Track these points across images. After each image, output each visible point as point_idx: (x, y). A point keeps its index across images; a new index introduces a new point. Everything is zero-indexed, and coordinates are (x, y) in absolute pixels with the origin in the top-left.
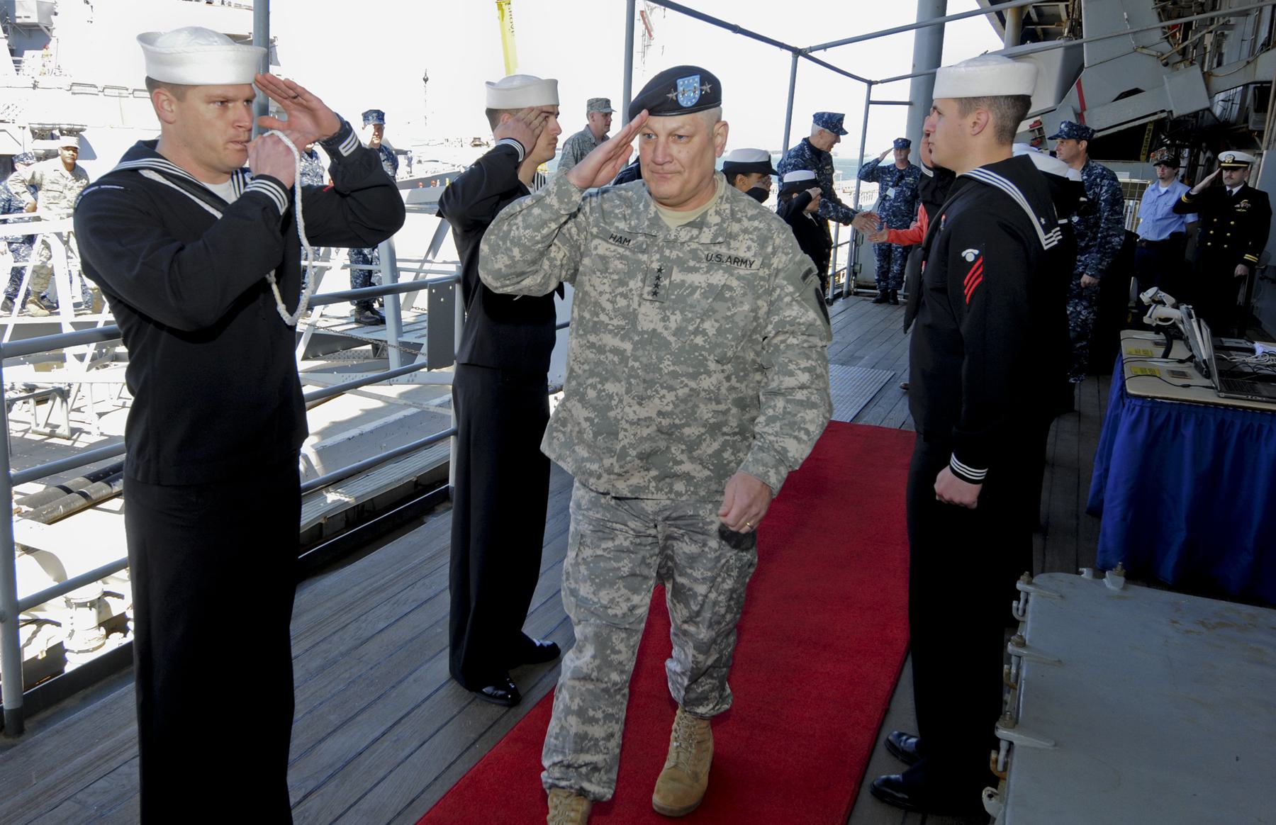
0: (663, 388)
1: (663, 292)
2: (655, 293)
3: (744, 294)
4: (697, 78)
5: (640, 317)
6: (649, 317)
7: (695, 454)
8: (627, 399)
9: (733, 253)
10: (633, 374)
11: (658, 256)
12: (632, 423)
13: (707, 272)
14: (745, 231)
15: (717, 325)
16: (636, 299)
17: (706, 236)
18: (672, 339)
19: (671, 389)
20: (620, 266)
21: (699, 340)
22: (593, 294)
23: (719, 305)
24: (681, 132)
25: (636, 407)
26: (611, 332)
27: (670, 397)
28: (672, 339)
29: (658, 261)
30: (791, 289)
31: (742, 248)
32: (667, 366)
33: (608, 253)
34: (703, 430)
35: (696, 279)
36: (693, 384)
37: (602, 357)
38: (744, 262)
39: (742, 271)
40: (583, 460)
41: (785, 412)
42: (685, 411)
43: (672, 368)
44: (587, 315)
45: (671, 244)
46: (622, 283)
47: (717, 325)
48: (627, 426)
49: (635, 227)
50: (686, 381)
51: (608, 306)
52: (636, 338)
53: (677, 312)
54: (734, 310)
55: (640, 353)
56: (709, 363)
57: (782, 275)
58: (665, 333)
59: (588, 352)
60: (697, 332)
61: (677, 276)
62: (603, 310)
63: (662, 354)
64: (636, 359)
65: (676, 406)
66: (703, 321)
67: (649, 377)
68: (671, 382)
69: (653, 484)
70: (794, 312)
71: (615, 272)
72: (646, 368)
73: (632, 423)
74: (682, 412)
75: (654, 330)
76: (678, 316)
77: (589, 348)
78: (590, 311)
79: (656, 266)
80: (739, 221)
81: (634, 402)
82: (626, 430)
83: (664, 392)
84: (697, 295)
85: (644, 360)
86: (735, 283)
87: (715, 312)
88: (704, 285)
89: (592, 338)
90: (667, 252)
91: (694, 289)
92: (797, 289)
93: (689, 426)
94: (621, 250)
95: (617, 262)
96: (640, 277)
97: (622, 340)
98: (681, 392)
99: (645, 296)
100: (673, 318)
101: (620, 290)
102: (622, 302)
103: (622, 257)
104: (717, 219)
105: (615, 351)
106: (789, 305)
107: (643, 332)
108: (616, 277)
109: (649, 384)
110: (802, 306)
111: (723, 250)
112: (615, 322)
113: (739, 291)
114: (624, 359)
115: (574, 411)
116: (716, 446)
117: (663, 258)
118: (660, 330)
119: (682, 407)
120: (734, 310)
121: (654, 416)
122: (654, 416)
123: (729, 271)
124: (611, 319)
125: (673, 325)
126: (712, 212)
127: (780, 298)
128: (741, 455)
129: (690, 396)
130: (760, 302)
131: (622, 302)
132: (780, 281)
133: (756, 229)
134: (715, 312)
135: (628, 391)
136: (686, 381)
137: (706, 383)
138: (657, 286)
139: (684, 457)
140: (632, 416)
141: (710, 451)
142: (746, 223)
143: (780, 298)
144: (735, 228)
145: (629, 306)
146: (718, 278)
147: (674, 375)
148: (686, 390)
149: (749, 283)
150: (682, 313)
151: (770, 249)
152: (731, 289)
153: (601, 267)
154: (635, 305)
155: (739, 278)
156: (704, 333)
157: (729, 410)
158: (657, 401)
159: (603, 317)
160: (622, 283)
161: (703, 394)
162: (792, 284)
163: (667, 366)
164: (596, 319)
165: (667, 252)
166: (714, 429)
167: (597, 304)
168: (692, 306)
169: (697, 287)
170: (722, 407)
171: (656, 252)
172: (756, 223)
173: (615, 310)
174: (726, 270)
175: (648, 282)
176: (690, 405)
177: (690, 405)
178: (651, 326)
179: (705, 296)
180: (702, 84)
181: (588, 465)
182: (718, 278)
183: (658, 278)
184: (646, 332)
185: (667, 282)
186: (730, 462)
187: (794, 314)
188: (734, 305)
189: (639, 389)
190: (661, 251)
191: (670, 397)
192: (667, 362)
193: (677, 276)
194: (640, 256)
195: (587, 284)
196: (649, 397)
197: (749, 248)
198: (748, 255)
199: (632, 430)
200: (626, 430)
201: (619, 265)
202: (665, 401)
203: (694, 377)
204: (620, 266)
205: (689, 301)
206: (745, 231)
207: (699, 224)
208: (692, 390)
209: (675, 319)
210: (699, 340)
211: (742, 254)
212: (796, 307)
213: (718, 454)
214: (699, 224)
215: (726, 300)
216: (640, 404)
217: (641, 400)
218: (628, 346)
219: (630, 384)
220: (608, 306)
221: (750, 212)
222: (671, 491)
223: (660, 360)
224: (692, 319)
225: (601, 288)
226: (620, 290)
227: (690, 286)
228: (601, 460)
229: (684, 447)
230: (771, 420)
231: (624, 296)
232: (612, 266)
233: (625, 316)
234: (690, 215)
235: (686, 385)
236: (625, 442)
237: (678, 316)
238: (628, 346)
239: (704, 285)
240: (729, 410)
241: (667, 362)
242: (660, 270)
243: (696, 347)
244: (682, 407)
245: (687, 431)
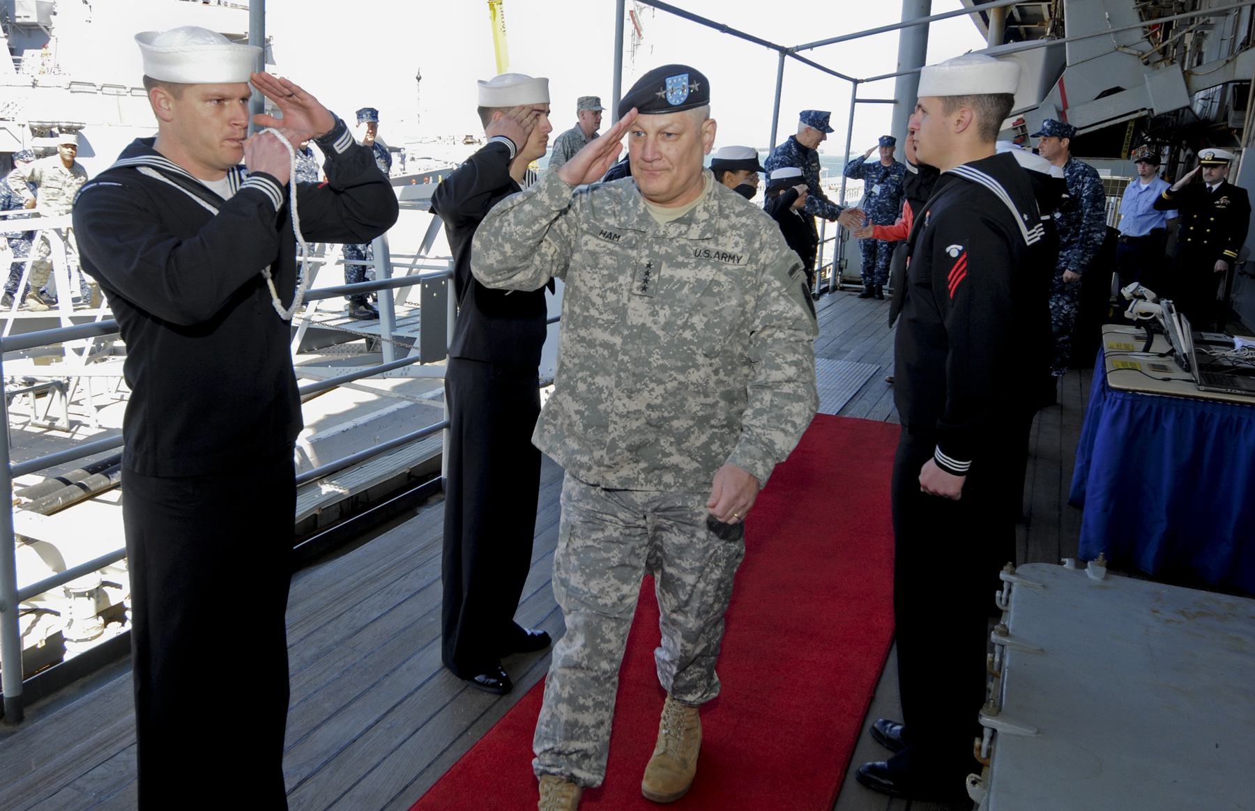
0: (652, 381)
1: (652, 287)
2: (644, 289)
3: (732, 289)
4: (686, 77)
5: (630, 311)
6: (638, 312)
7: (684, 446)
8: (616, 392)
9: (720, 248)
10: (622, 368)
11: (647, 252)
12: (621, 416)
13: (696, 267)
14: (733, 227)
15: (705, 319)
16: (626, 294)
17: (695, 232)
18: (661, 333)
19: (660, 382)
20: (610, 262)
21: (688, 335)
22: (584, 289)
23: (707, 300)
24: (670, 130)
25: (626, 401)
26: (600, 326)
27: (659, 390)
28: (661, 333)
29: (647, 256)
30: (778, 284)
31: (730, 243)
32: (656, 359)
33: (598, 249)
34: (691, 423)
35: (685, 274)
36: (681, 378)
38: (732, 257)
39: (730, 266)
40: (574, 452)
41: (772, 405)
42: (674, 404)
43: (660, 362)
44: (577, 310)
45: (660, 239)
46: (612, 278)
47: (705, 319)
48: (617, 419)
50: (675, 375)
51: (598, 301)
52: (626, 332)
53: (666, 307)
54: (722, 305)
55: (629, 347)
56: (698, 357)
57: (769, 270)
58: (654, 328)
59: (578, 346)
60: (685, 326)
61: (666, 271)
62: (593, 305)
63: (652, 348)
64: (625, 353)
65: (665, 399)
66: (691, 315)
67: (638, 371)
68: (660, 376)
69: (642, 476)
70: (780, 306)
71: (605, 267)
72: (636, 362)
73: (621, 416)
74: (670, 405)
75: (644, 325)
76: (667, 311)
77: (579, 342)
78: (580, 306)
79: (645, 261)
80: (727, 217)
81: (624, 396)
82: (615, 423)
83: (653, 385)
84: (686, 290)
85: (634, 354)
86: (723, 278)
87: (703, 306)
88: (692, 280)
89: (583, 333)
90: (656, 248)
91: (682, 284)
92: (784, 284)
93: (678, 418)
94: (611, 246)
95: (607, 258)
96: (629, 272)
97: (612, 334)
98: (670, 386)
99: (635, 291)
100: (662, 313)
101: (610, 285)
102: (611, 297)
103: (612, 253)
104: (705, 216)
105: (605, 345)
106: (776, 300)
107: (633, 326)
108: (605, 272)
109: (639, 377)
110: (788, 301)
111: (711, 246)
112: (605, 317)
113: (727, 286)
114: (614, 353)
116: (704, 438)
117: (652, 254)
118: (649, 324)
119: (671, 400)
120: (722, 305)
121: (643, 409)
122: (643, 409)
123: (717, 267)
124: (601, 313)
125: (662, 320)
126: (700, 208)
127: (767, 293)
128: (729, 447)
129: (679, 389)
130: (747, 297)
131: (611, 297)
132: (767, 276)
133: (744, 225)
134: (703, 306)
135: (618, 385)
136: (675, 375)
137: (695, 376)
138: (646, 281)
139: (672, 449)
140: (621, 409)
141: (698, 443)
142: (733, 219)
143: (767, 293)
144: (723, 224)
145: (618, 301)
146: (707, 273)
147: (663, 368)
148: (675, 384)
149: (737, 278)
150: (671, 308)
151: (757, 245)
152: (719, 284)
153: (591, 263)
154: (625, 300)
155: (727, 273)
156: (692, 327)
157: (717, 403)
158: (646, 394)
159: (593, 312)
160: (612, 278)
161: (691, 387)
162: (779, 279)
163: (656, 359)
164: (586, 314)
165: (656, 248)
166: (702, 422)
167: (587, 299)
168: (680, 301)
169: (686, 282)
170: (710, 400)
171: (646, 248)
172: (744, 220)
173: (605, 305)
174: (714, 266)
175: (637, 277)
176: (679, 398)
177: (679, 398)
178: (641, 321)
179: (693, 291)
180: (690, 82)
182: (707, 273)
183: (647, 273)
184: (635, 326)
185: (656, 277)
186: (718, 454)
187: (781, 308)
188: (722, 300)
189: (628, 383)
190: (650, 246)
191: (659, 390)
192: (656, 356)
193: (666, 271)
194: (630, 251)
195: (578, 279)
196: (639, 391)
197: (736, 244)
198: (736, 251)
199: (621, 422)
200: (615, 423)
201: (609, 261)
202: (654, 394)
203: (683, 370)
204: (610, 262)
205: (678, 296)
206: (733, 227)
207: (688, 220)
208: (680, 383)
209: (664, 314)
210: (688, 335)
211: (730, 250)
212: (783, 302)
213: (706, 446)
214: (688, 220)
215: (714, 295)
216: (630, 397)
217: (630, 394)
218: (617, 340)
219: (620, 377)
220: (598, 301)
221: (738, 209)
222: (660, 483)
223: (650, 353)
224: (681, 314)
225: (591, 283)
226: (610, 285)
227: (679, 281)
229: (672, 439)
230: (759, 413)
231: (614, 291)
232: (602, 261)
233: (614, 311)
234: (679, 211)
235: (675, 379)
236: (615, 434)
237: (667, 311)
238: (617, 340)
239: (692, 280)
240: (717, 403)
241: (656, 356)
242: (649, 266)
243: (684, 341)
244: (671, 400)
245: (675, 424)
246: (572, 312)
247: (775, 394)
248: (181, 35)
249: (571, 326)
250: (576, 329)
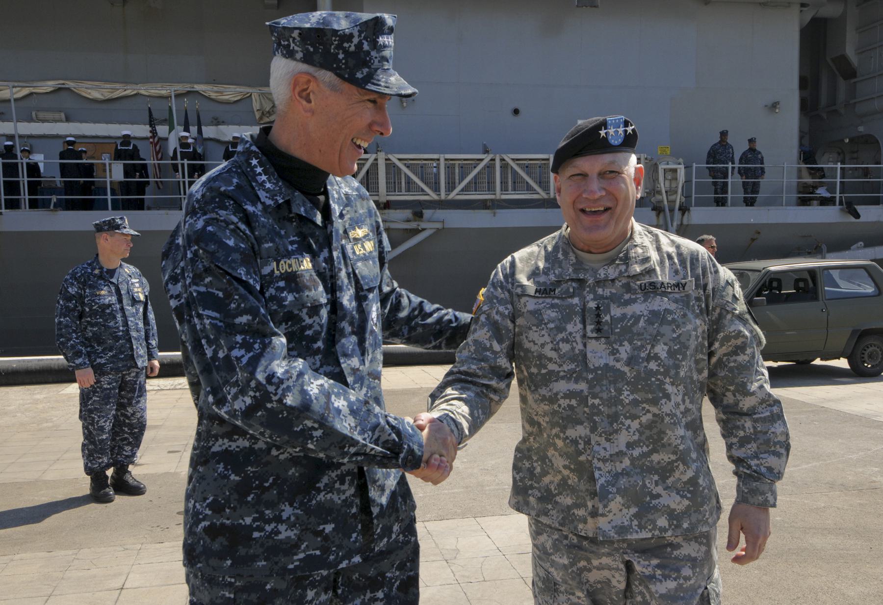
0: (626, 418)
1: (606, 328)
2: (598, 330)
5: (589, 355)
6: (598, 353)
7: (670, 481)
11: (591, 296)
12: (604, 460)
13: (645, 301)
15: (666, 348)
18: (626, 369)
19: (634, 417)
20: (554, 315)
21: (653, 366)
22: (534, 348)
23: (666, 329)
25: (607, 445)
26: (563, 378)
27: (635, 425)
28: (626, 369)
29: (594, 300)
32: (627, 396)
33: (537, 307)
34: (673, 457)
35: (638, 308)
36: (655, 410)
37: (555, 407)
40: (569, 508)
41: (756, 432)
42: (651, 437)
43: (631, 397)
44: (534, 370)
46: (560, 329)
47: (666, 348)
48: (600, 464)
49: (560, 275)
50: (647, 407)
51: (553, 355)
52: (590, 376)
53: (626, 343)
54: (679, 332)
56: (667, 387)
58: (618, 365)
59: (542, 405)
60: (649, 359)
61: (616, 311)
62: (550, 360)
63: (620, 385)
64: (595, 396)
65: (641, 434)
66: (653, 346)
69: (635, 522)
71: (550, 321)
73: (604, 460)
74: (648, 438)
75: (606, 365)
76: (627, 346)
77: (542, 401)
78: (536, 366)
79: (592, 305)
81: (602, 440)
82: (600, 469)
83: (628, 422)
84: (642, 323)
87: (663, 335)
88: (646, 313)
89: (543, 391)
90: (600, 291)
91: (637, 318)
93: (658, 452)
94: (549, 300)
95: (549, 312)
96: (578, 319)
97: (576, 382)
98: (644, 419)
99: (589, 334)
100: (622, 350)
101: (560, 336)
102: (565, 347)
103: (553, 306)
105: (570, 395)
107: (597, 369)
108: (552, 325)
112: (566, 367)
114: (583, 400)
115: (553, 460)
118: (612, 363)
119: (648, 433)
120: (679, 332)
124: (560, 366)
125: (624, 356)
129: (653, 422)
131: (565, 347)
134: (663, 335)
135: (593, 429)
136: (647, 407)
138: (599, 323)
139: (659, 489)
140: (603, 453)
141: (685, 478)
145: (573, 349)
147: (635, 403)
148: (649, 416)
150: (630, 343)
153: (535, 322)
154: (580, 346)
156: (656, 357)
158: (624, 432)
159: (552, 367)
160: (560, 329)
161: (667, 419)
164: (544, 371)
165: (600, 291)
167: (541, 357)
168: (639, 334)
169: (640, 316)
171: (589, 292)
173: (560, 357)
175: (588, 321)
176: (655, 431)
177: (655, 431)
179: (650, 322)
181: (645, 449)
183: (598, 316)
184: (599, 368)
185: (608, 318)
188: (678, 327)
190: (593, 291)
191: (635, 425)
192: (626, 393)
194: (570, 300)
195: (525, 341)
196: (616, 431)
199: (608, 466)
200: (600, 469)
201: (553, 314)
202: (632, 431)
203: (655, 402)
204: (554, 315)
205: (635, 330)
208: (654, 415)
209: (625, 350)
210: (653, 366)
215: (670, 323)
216: (608, 440)
218: (582, 386)
219: (595, 422)
220: (553, 355)
222: (655, 527)
223: (619, 391)
224: (642, 346)
225: (541, 341)
226: (560, 336)
227: (632, 316)
228: (632, 463)
229: (656, 477)
231: (566, 340)
232: (545, 317)
233: (573, 359)
235: (648, 411)
236: (602, 481)
237: (627, 346)
238: (582, 386)
239: (646, 313)
241: (626, 393)
242: (598, 308)
243: (650, 373)
246: (531, 374)
247: (756, 421)
248: (4, 138)
249: (533, 388)
250: (536, 390)
